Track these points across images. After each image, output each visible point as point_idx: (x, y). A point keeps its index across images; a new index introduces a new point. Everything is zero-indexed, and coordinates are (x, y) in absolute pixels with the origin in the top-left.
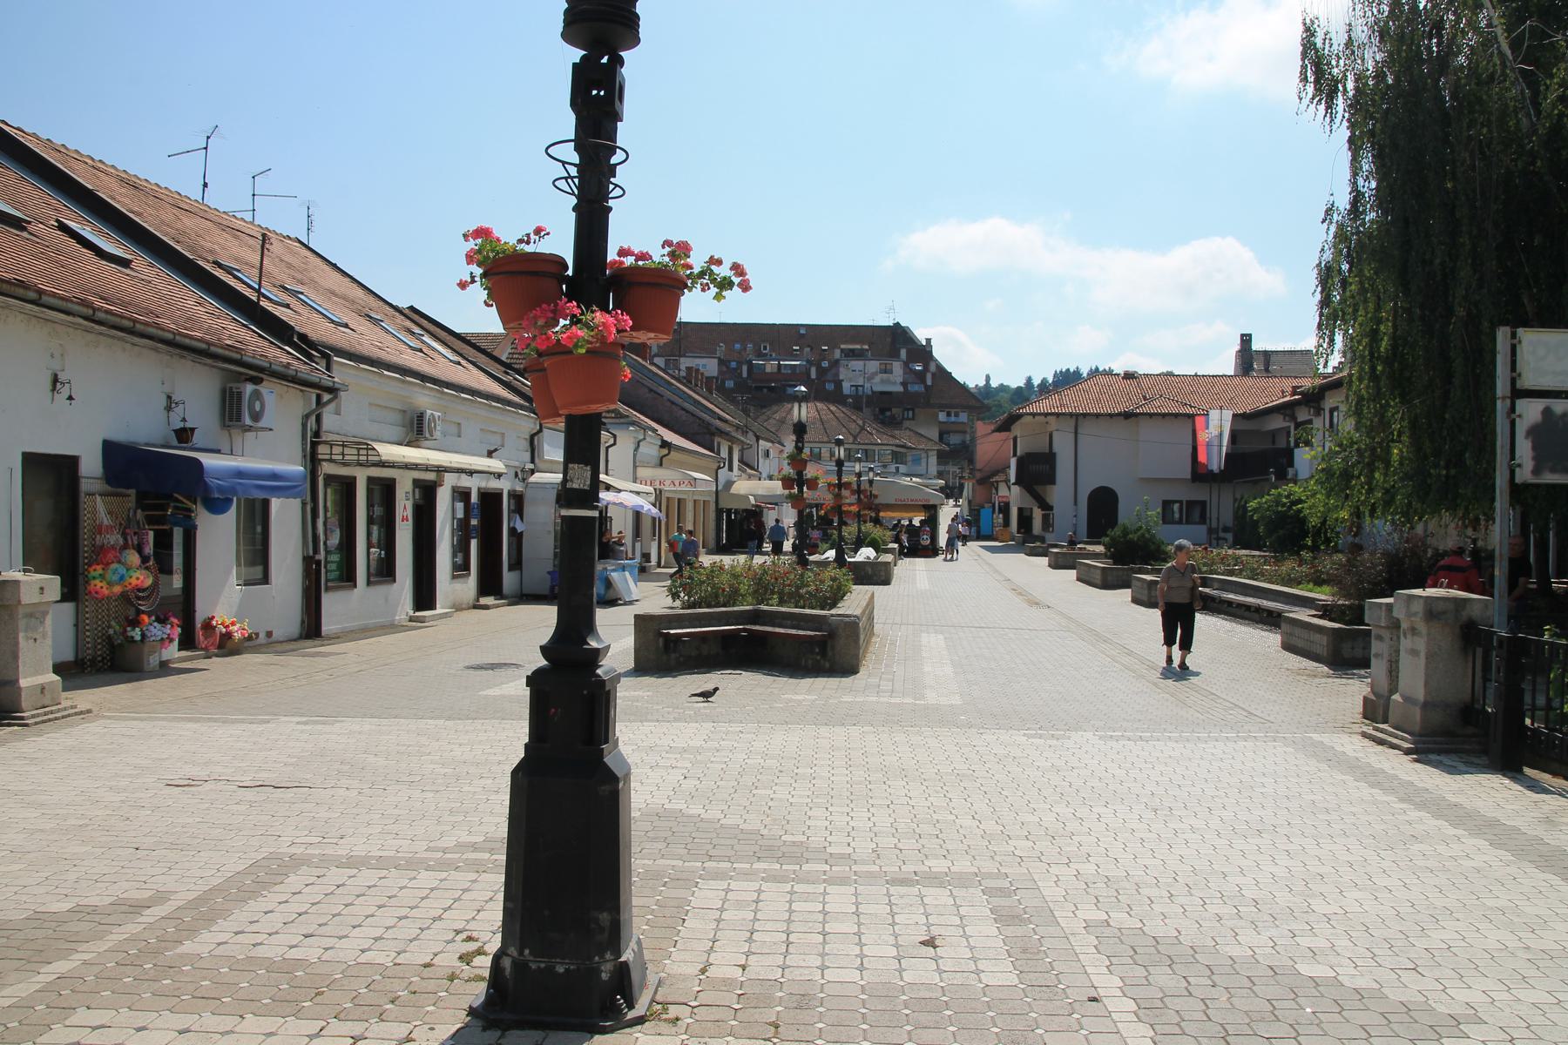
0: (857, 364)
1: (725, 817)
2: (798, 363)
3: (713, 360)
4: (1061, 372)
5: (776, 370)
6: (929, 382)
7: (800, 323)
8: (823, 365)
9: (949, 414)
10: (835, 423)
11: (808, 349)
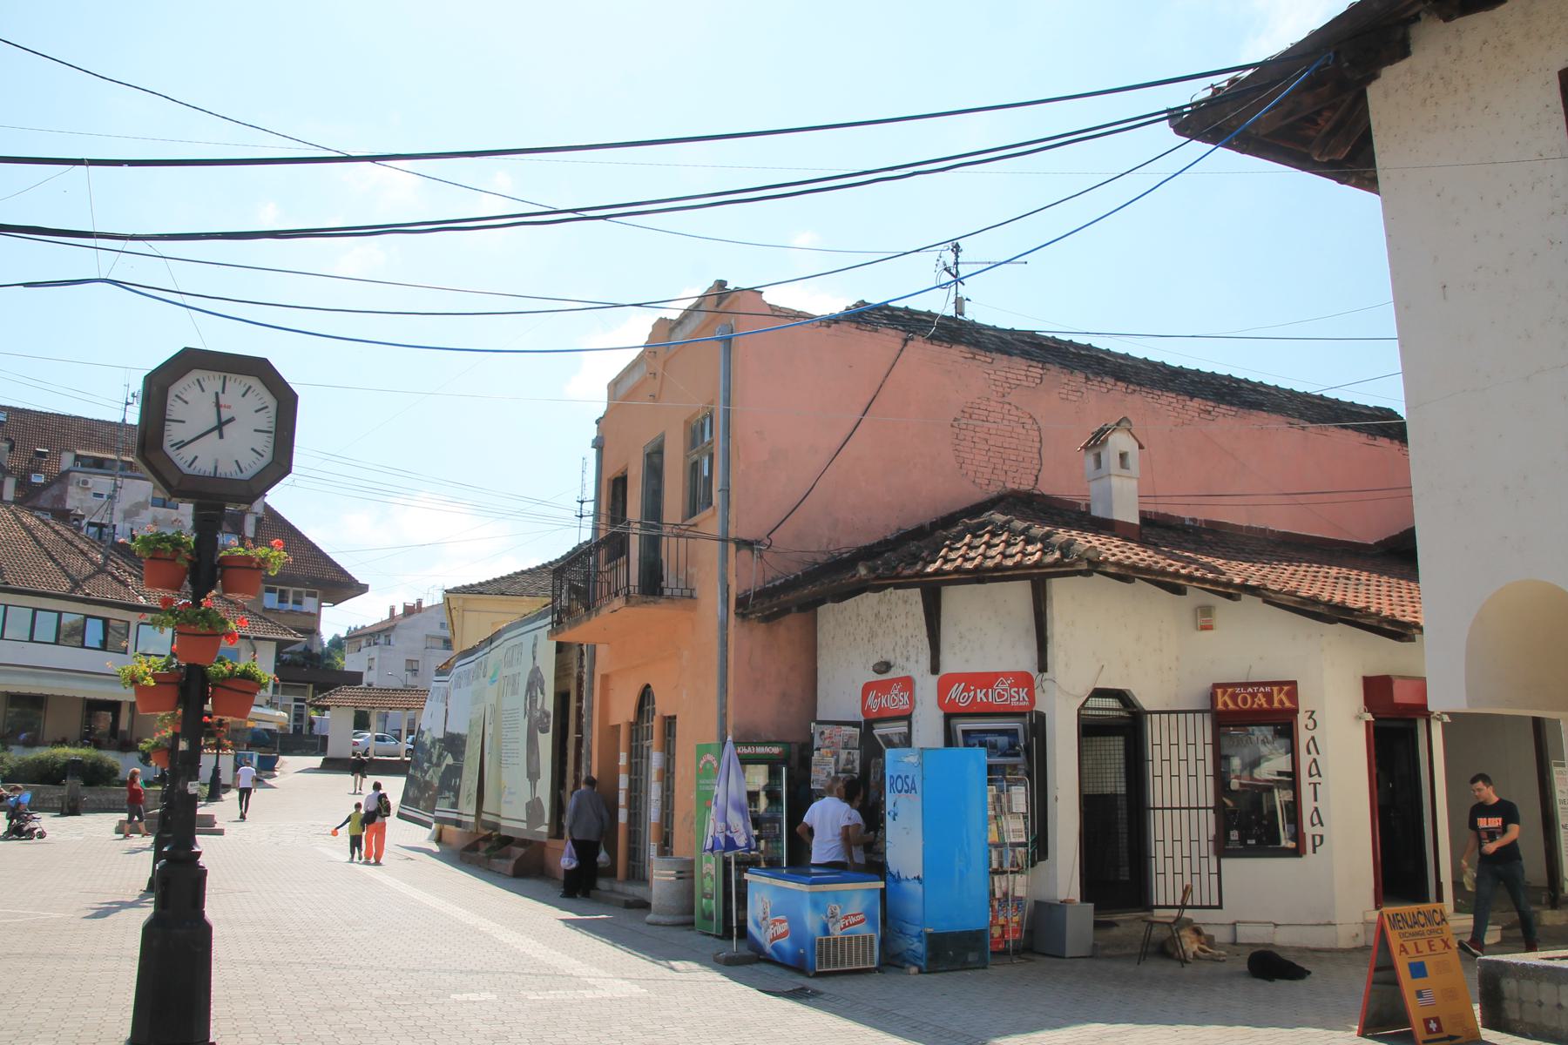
0: (102, 483)
4: (355, 629)
9: (283, 598)
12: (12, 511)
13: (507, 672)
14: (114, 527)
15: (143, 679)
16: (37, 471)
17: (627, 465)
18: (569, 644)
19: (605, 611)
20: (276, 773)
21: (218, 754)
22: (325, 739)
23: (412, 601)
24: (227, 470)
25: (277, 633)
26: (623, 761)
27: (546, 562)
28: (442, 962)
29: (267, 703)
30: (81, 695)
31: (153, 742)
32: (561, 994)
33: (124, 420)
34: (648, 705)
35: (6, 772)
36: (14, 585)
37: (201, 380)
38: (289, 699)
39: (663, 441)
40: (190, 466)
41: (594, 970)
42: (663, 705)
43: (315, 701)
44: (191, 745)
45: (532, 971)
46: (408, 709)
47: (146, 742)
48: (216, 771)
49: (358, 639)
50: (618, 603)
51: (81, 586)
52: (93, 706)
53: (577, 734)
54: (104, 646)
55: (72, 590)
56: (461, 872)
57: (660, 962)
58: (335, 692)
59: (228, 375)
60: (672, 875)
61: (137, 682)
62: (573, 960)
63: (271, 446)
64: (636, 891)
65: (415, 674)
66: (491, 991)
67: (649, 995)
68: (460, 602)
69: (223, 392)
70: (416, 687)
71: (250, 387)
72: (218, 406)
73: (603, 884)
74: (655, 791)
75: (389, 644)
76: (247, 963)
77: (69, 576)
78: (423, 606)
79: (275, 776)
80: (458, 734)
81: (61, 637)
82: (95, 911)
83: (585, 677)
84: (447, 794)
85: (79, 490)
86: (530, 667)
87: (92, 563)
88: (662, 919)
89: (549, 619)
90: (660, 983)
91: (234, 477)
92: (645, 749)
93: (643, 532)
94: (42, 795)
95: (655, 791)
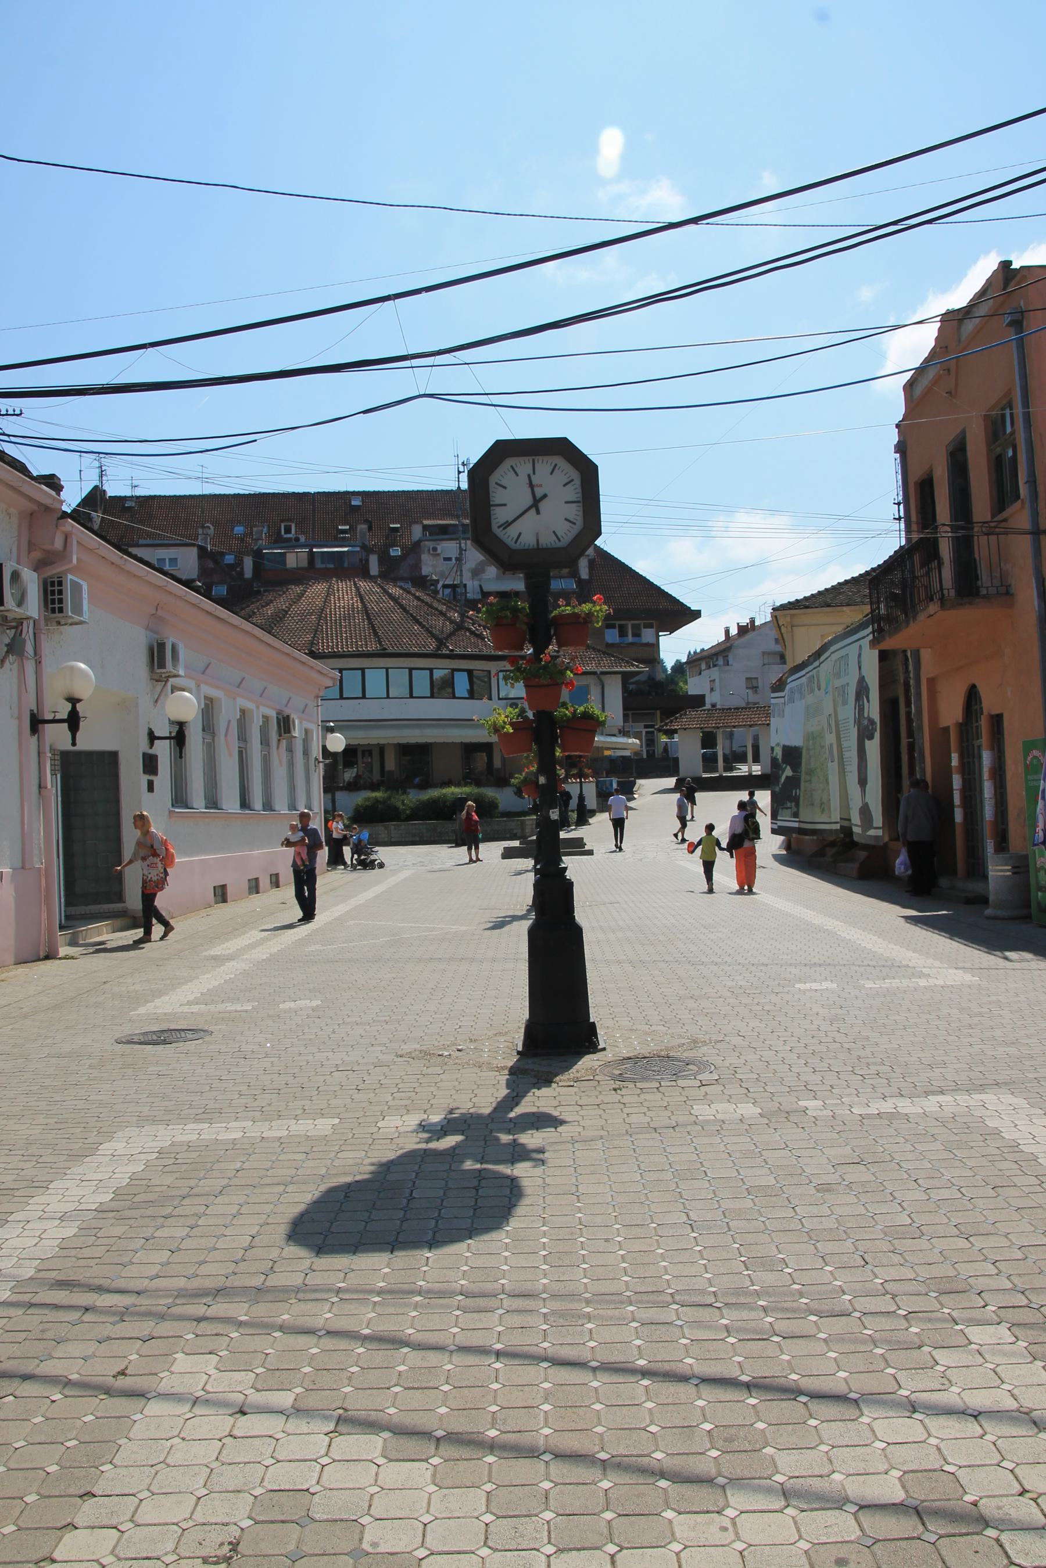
1: (352, 1138)
2: (346, 549)
3: (192, 548)
4: (695, 652)
5: (304, 564)
6: (584, 573)
7: (351, 490)
8: (392, 553)
9: (623, 633)
10: (397, 615)
11: (364, 527)
12: (379, 585)
13: (838, 683)
14: (465, 585)
15: (504, 728)
16: (394, 545)
17: (931, 466)
18: (894, 652)
19: (921, 617)
20: (635, 796)
21: (581, 782)
22: (676, 760)
23: (745, 621)
24: (547, 540)
25: (621, 666)
26: (955, 762)
27: (868, 569)
28: (789, 957)
29: (620, 732)
30: (458, 740)
31: (522, 777)
32: (896, 983)
33: (459, 487)
34: (976, 704)
35: (408, 812)
36: (390, 650)
37: (514, 466)
38: (640, 727)
39: (964, 438)
40: (516, 542)
41: (930, 961)
42: (989, 704)
43: (663, 726)
44: (548, 779)
45: (871, 963)
46: (751, 726)
47: (517, 778)
48: (581, 798)
49: (697, 663)
50: (933, 608)
51: (445, 644)
52: (470, 749)
53: (908, 738)
54: (472, 695)
55: (438, 648)
56: (810, 877)
57: (995, 953)
58: (681, 715)
59: (536, 458)
60: (1008, 871)
61: (499, 731)
62: (911, 952)
63: (581, 514)
64: (974, 887)
65: (756, 691)
66: (832, 981)
67: (980, 982)
68: (788, 619)
69: (534, 473)
70: (758, 703)
71: (556, 465)
72: (531, 486)
73: (944, 882)
74: (988, 790)
75: (728, 665)
76: (619, 962)
77: (433, 636)
78: (756, 624)
79: (635, 799)
80: (795, 747)
81: (435, 690)
82: (492, 924)
83: (912, 682)
84: (789, 804)
85: (431, 558)
86: (857, 678)
87: (452, 622)
88: (1000, 913)
89: (870, 629)
90: (993, 972)
91: (554, 546)
92: (976, 748)
93: (954, 535)
94: (439, 830)
95: (988, 790)
